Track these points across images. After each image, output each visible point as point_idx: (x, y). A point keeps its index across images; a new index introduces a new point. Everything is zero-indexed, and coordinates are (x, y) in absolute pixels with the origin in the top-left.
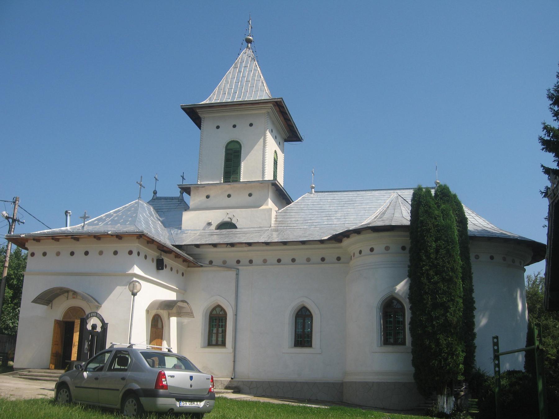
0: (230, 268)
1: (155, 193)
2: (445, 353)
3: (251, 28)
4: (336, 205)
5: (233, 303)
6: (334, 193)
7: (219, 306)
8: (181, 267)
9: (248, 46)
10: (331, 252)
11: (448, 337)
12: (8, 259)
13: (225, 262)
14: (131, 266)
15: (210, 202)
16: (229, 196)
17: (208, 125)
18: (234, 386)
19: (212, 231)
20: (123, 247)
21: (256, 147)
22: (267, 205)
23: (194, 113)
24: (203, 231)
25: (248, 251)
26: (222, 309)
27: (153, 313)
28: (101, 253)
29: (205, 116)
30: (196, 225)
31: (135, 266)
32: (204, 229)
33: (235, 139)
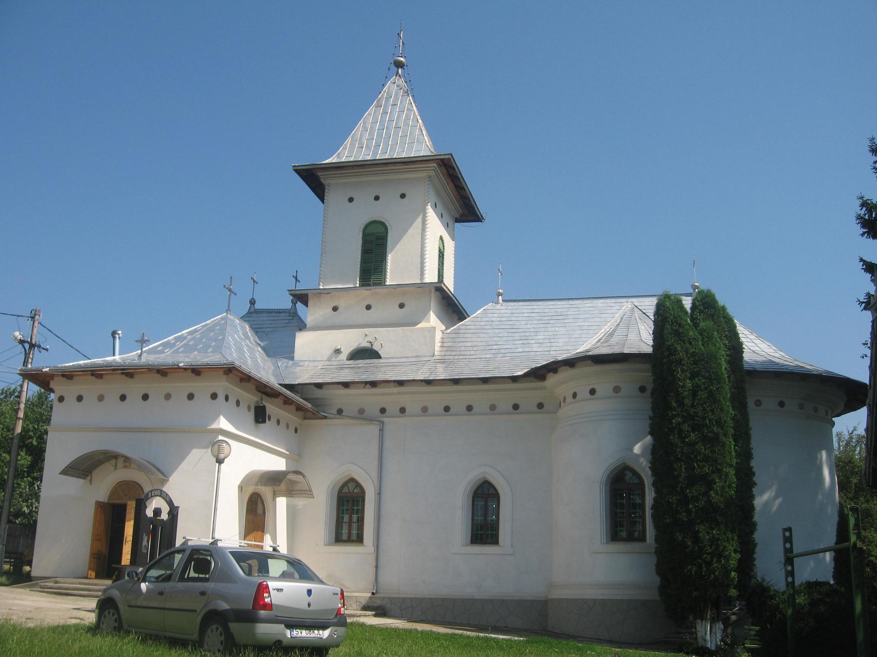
0: (370, 420)
1: (252, 302)
3: (403, 44)
5: (374, 475)
6: (533, 303)
7: (352, 480)
9: (397, 73)
11: (712, 529)
13: (361, 411)
14: (216, 418)
15: (338, 318)
18: (376, 605)
19: (342, 363)
20: (202, 387)
23: (314, 178)
25: (399, 393)
26: (358, 485)
28: (168, 397)
30: (317, 352)
32: (329, 360)
33: (377, 219)
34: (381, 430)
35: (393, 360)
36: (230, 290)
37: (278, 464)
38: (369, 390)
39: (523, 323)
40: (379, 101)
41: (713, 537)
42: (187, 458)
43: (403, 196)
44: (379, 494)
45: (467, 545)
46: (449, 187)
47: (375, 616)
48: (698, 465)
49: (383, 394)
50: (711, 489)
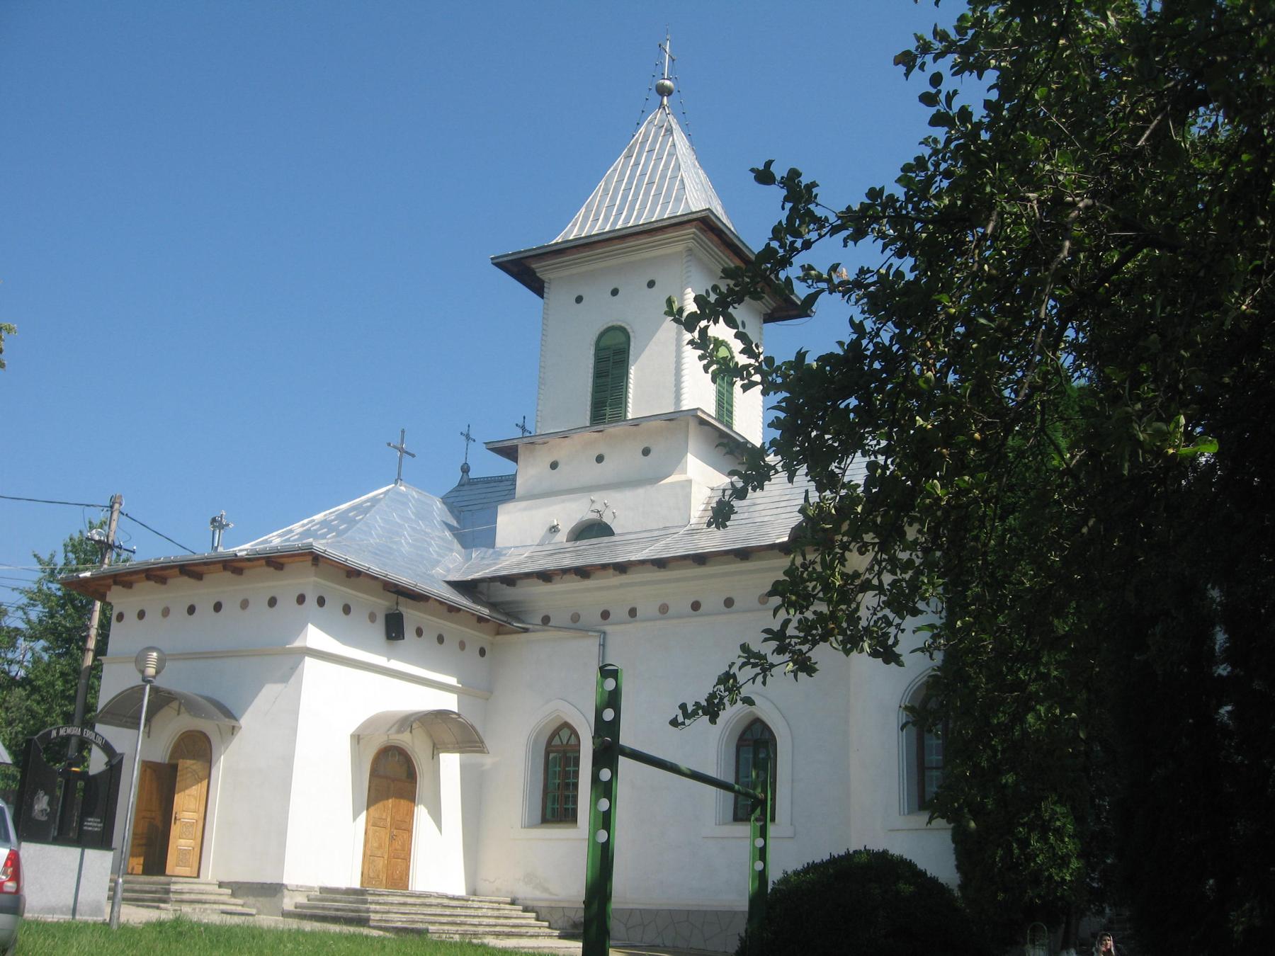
0: (585, 630)
1: (465, 469)
8: (477, 637)
9: (662, 103)
12: (93, 632)
13: (576, 618)
14: (300, 629)
16: (600, 459)
17: (559, 295)
22: (684, 471)
23: (525, 269)
24: (540, 548)
25: (621, 586)
26: (574, 732)
28: (245, 604)
29: (551, 276)
30: (525, 532)
31: (310, 626)
33: (614, 324)
34: (603, 646)
36: (402, 450)
37: (450, 702)
38: (577, 584)
45: (725, 824)
46: (631, 243)
47: (560, 937)
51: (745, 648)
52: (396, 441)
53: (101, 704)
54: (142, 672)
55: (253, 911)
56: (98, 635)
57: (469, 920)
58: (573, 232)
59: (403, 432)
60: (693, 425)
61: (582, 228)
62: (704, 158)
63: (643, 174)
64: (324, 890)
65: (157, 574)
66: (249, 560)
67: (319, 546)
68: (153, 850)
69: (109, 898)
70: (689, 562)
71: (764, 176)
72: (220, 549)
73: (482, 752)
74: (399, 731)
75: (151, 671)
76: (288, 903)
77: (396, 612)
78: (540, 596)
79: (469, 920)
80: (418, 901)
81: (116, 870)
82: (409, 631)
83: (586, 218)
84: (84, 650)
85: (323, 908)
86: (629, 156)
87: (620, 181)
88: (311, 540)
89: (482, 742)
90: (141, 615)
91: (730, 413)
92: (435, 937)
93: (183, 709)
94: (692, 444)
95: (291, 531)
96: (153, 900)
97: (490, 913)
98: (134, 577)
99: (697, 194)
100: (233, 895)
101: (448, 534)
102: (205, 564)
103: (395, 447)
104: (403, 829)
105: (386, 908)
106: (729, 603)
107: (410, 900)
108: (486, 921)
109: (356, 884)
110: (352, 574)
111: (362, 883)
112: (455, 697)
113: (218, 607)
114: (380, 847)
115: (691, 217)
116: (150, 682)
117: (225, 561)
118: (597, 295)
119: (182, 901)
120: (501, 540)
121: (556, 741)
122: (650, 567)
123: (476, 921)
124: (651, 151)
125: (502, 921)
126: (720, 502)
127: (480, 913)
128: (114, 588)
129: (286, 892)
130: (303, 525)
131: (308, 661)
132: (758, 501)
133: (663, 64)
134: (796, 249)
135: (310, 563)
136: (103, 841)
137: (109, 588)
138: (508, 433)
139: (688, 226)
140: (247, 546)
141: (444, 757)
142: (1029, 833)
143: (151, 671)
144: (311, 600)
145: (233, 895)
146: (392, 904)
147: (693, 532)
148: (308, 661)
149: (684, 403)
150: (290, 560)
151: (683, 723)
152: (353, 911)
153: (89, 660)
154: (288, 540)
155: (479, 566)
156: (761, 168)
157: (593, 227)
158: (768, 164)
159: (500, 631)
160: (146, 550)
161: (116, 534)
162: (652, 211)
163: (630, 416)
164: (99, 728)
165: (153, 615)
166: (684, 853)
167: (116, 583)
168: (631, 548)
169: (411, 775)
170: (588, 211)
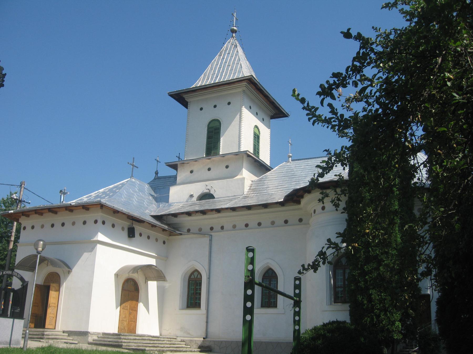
0: (204, 234)
1: (157, 173)
2: (378, 309)
3: (237, 20)
4: (307, 171)
5: (207, 267)
6: (309, 160)
7: (196, 270)
8: (162, 236)
9: (233, 36)
10: (291, 212)
11: (381, 292)
12: (13, 234)
13: (200, 230)
14: (96, 234)
15: (195, 176)
16: (209, 169)
17: (194, 107)
18: (206, 345)
19: (193, 202)
20: (90, 216)
21: (233, 123)
23: (181, 98)
25: (218, 217)
26: (199, 273)
27: (125, 276)
28: (74, 224)
30: (181, 196)
32: (187, 201)
34: (211, 240)
35: (221, 199)
36: (133, 165)
37: (152, 262)
38: (201, 217)
39: (300, 172)
40: (221, 53)
41: (381, 298)
42: (81, 258)
43: (229, 103)
44: (209, 278)
46: (260, 97)
48: (372, 249)
49: (210, 219)
50: (381, 265)
51: (329, 240)
52: (131, 162)
53: (17, 261)
54: (37, 249)
55: (76, 342)
56: (15, 235)
57: (160, 345)
58: (199, 83)
59: (134, 158)
60: (245, 156)
61: (202, 82)
62: (248, 58)
63: (226, 62)
64: (104, 334)
65: (39, 212)
66: (76, 206)
67: (103, 201)
68: (39, 320)
69: (22, 338)
70: (278, 205)
71: (347, 35)
72: (64, 202)
73: (164, 281)
74: (133, 273)
75: (40, 249)
76: (90, 339)
77: (132, 227)
78: (186, 221)
79: (160, 345)
80: (140, 338)
81: (25, 327)
82: (137, 234)
83: (204, 79)
84: (8, 242)
85: (104, 341)
86: (220, 55)
87: (217, 65)
88: (99, 199)
89: (165, 277)
90: (33, 227)
91: (258, 153)
92: (148, 352)
93: (49, 264)
94: (245, 164)
95: (91, 196)
96: (38, 338)
97: (168, 342)
98: (43, 211)
99: (246, 71)
100: (69, 336)
101: (151, 197)
102: (59, 208)
103: (131, 164)
104: (135, 310)
105: (129, 341)
106: (259, 224)
107: (137, 338)
108: (166, 346)
109: (116, 332)
110: (116, 212)
111: (118, 332)
112: (155, 260)
113: (63, 224)
114: (125, 317)
115: (245, 78)
116: (40, 253)
117: (66, 207)
118: (208, 107)
119: (49, 339)
120: (171, 200)
121: (193, 277)
122: (230, 210)
123: (162, 345)
124: (229, 53)
125: (172, 346)
126: (312, 179)
127: (164, 342)
128: (23, 217)
129: (89, 335)
130: (96, 194)
131: (99, 246)
132: (270, 186)
133: (233, 21)
134: (365, 66)
135: (99, 208)
136: (20, 316)
137: (20, 217)
138: (174, 159)
139: (243, 82)
140: (74, 201)
141: (150, 282)
142: (380, 312)
143: (40, 249)
144: (100, 222)
145: (69, 336)
146: (131, 339)
147: (245, 197)
148: (99, 246)
149: (241, 148)
150: (92, 206)
151: (303, 273)
152: (116, 342)
153: (11, 246)
154: (90, 199)
155: (163, 210)
156: (346, 31)
157: (207, 81)
158: (349, 30)
159: (171, 234)
160: (33, 203)
161: (23, 195)
162: (230, 76)
163: (221, 153)
164: (15, 270)
165: (37, 227)
166: (273, 324)
167: (23, 215)
168: (223, 203)
169: (137, 289)
170: (205, 76)
